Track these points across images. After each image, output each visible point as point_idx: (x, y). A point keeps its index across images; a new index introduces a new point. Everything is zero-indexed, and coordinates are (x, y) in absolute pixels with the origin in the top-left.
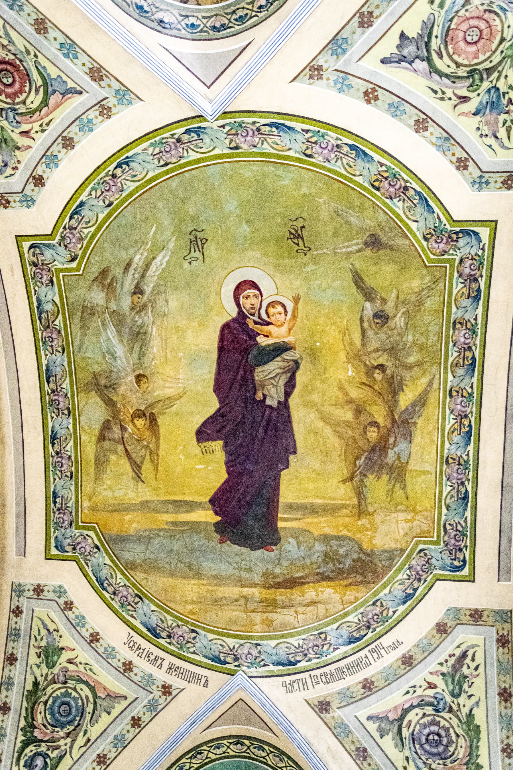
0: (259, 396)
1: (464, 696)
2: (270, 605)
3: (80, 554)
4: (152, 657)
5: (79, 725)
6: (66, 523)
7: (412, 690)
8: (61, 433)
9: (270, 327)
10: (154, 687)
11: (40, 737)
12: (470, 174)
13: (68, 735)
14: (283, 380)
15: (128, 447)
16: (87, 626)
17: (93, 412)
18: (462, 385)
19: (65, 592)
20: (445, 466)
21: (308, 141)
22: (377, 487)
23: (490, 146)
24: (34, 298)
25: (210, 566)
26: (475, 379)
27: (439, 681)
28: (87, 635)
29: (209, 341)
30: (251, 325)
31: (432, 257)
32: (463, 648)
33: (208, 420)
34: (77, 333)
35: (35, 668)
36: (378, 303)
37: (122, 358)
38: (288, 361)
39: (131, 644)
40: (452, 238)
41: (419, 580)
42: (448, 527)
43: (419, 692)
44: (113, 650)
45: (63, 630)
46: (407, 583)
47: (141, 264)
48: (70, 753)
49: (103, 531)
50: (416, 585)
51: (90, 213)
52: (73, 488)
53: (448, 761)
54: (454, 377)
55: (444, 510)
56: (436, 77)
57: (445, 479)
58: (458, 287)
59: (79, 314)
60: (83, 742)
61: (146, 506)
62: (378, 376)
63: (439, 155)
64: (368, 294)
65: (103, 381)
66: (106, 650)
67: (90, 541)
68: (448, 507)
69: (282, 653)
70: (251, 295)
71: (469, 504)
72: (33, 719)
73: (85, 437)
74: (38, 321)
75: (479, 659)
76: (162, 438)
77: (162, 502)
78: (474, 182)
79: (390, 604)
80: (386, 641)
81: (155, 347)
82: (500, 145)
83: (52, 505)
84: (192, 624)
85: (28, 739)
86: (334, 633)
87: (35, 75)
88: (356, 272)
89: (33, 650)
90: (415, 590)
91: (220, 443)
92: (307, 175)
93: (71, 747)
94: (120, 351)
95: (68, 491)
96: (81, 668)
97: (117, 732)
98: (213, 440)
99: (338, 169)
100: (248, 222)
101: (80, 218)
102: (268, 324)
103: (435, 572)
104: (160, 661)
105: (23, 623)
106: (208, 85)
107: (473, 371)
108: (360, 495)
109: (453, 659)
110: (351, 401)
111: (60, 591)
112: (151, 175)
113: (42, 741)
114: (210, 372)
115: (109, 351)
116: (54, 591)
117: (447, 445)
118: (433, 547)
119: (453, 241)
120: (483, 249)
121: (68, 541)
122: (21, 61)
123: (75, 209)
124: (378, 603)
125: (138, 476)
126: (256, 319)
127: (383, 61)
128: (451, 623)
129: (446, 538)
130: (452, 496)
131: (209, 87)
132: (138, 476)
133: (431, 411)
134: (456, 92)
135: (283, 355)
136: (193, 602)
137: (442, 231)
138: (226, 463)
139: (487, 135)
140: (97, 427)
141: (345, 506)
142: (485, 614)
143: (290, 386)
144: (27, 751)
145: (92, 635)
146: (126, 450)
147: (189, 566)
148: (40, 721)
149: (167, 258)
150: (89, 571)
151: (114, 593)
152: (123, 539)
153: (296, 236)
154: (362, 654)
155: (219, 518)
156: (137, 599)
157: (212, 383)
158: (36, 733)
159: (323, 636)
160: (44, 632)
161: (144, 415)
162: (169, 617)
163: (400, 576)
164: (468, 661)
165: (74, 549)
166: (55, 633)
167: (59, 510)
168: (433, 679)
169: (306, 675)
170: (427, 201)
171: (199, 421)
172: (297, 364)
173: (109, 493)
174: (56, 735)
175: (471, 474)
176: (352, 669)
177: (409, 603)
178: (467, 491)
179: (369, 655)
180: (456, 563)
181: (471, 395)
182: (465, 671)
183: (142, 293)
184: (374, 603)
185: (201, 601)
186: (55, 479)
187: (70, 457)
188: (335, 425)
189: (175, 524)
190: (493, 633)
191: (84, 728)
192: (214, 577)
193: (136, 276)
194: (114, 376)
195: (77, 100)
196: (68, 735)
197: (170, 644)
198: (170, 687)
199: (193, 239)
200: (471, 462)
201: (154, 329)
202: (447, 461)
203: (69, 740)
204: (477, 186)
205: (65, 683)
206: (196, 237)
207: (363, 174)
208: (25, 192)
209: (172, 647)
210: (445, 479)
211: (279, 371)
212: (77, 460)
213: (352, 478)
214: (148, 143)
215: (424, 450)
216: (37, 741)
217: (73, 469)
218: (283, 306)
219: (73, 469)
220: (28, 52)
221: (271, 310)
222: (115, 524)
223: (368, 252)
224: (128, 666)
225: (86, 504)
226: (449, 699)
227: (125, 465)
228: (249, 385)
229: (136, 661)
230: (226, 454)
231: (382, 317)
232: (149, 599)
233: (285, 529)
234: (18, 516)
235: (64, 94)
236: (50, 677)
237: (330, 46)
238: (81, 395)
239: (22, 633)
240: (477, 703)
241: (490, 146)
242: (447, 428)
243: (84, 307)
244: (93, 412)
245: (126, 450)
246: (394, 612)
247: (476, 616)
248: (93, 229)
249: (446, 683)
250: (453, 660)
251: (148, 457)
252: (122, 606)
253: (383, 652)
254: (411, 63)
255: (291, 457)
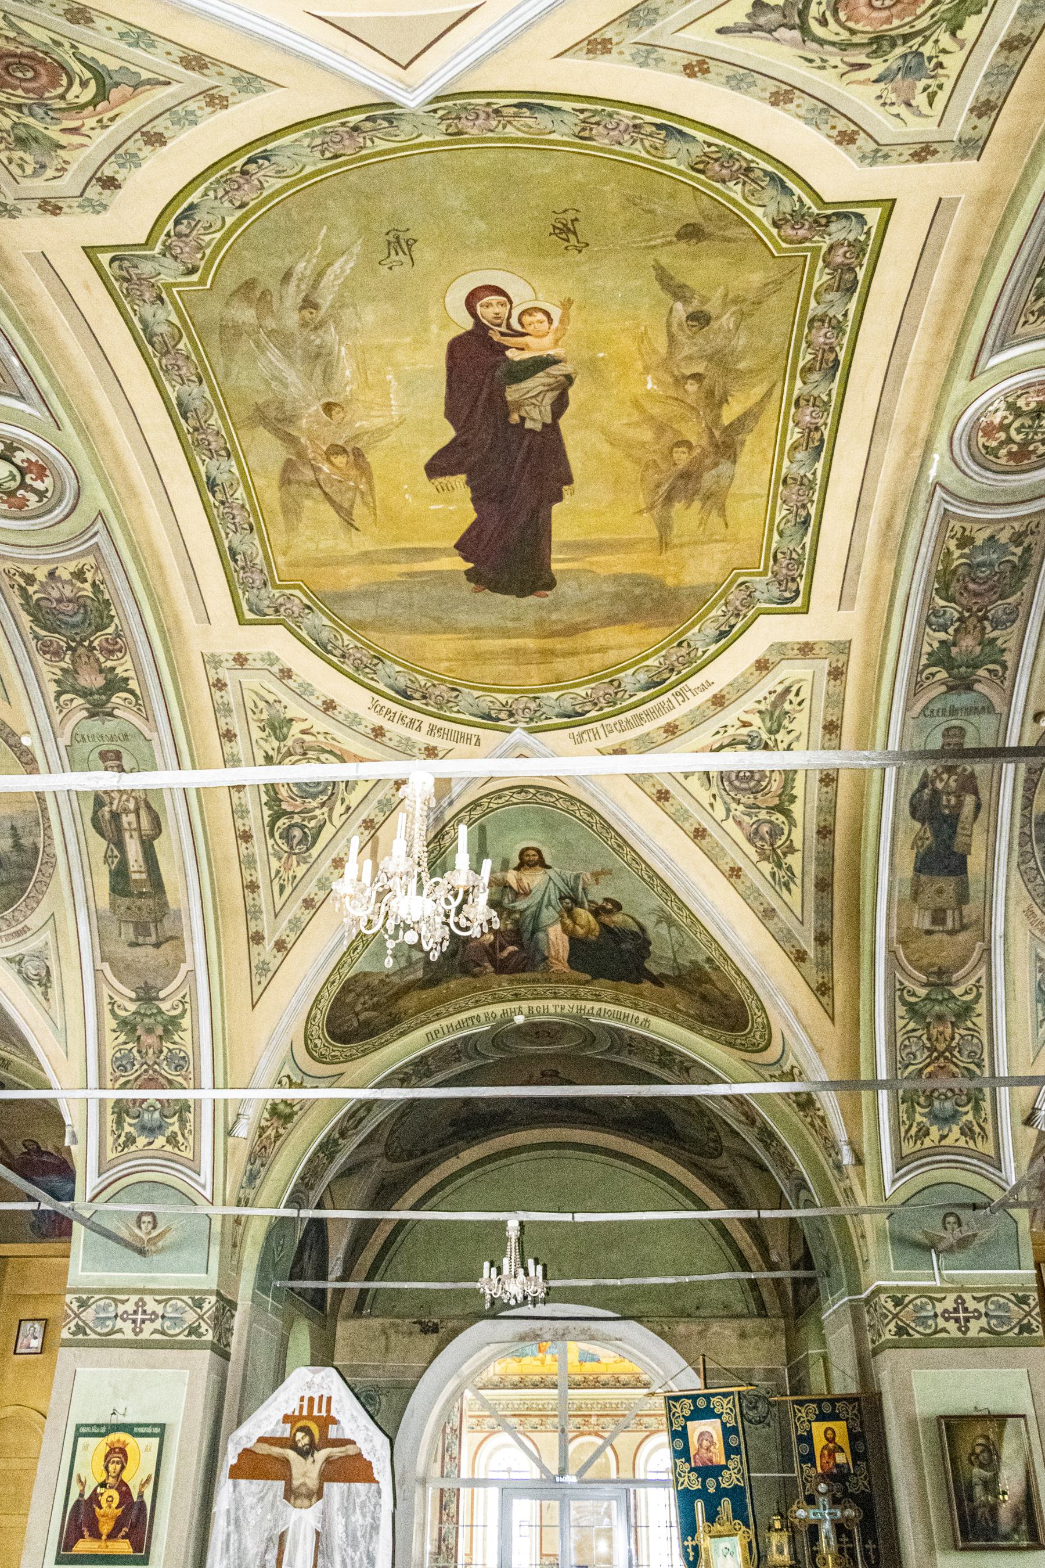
0: (515, 418)
1: (782, 731)
2: (546, 655)
3: (289, 616)
4: (407, 720)
5: (332, 794)
6: (258, 583)
7: (722, 731)
8: (222, 478)
9: (527, 339)
10: (416, 751)
11: (289, 809)
12: (859, 148)
13: (323, 804)
14: (550, 398)
15: (327, 490)
16: (316, 694)
17: (265, 452)
18: (815, 393)
19: (277, 659)
20: (781, 487)
21: (584, 122)
22: (686, 517)
23: (898, 116)
24: (136, 320)
25: (464, 618)
26: (835, 385)
27: (756, 720)
28: (319, 703)
29: (432, 364)
30: (497, 338)
31: (784, 245)
32: (787, 684)
33: (440, 451)
34: (220, 362)
35: (262, 742)
36: (696, 302)
37: (295, 383)
38: (555, 376)
39: (375, 707)
40: (821, 223)
41: (738, 615)
42: (779, 556)
43: (731, 731)
44: (356, 716)
45: (285, 700)
46: (722, 619)
47: (308, 272)
48: (331, 821)
49: (313, 588)
50: (733, 621)
51: (210, 218)
52: (257, 542)
53: (759, 795)
54: (805, 383)
55: (776, 537)
56: (814, 46)
57: (779, 501)
58: (822, 277)
59: (216, 337)
60: (343, 810)
61: (366, 557)
62: (692, 387)
63: (811, 130)
64: (679, 292)
65: (272, 413)
66: (347, 717)
67: (297, 601)
68: (781, 534)
69: (567, 704)
70: (494, 303)
71: (810, 529)
72: (276, 793)
73: (260, 482)
74: (149, 347)
75: (805, 694)
76: (375, 477)
77: (389, 551)
78: (864, 157)
79: (699, 644)
80: (693, 682)
81: (347, 370)
82: (913, 113)
83: (232, 564)
84: (452, 683)
85: (276, 812)
86: (630, 680)
87: (77, 67)
88: (662, 268)
89: (254, 726)
90: (732, 627)
91: (462, 478)
92: (583, 161)
93: (330, 817)
94: (291, 376)
95: (250, 546)
96: (321, 738)
97: (380, 796)
98: (452, 474)
99: (636, 153)
100: (482, 217)
101: (193, 223)
102: (523, 335)
103: (758, 605)
104: (417, 724)
105: (231, 696)
106: (404, 64)
107: (834, 375)
108: (664, 527)
109: (774, 696)
110: (652, 418)
111: (271, 660)
112: (308, 170)
113: (293, 812)
114: (437, 395)
115: (275, 378)
116: (263, 660)
117: (786, 462)
118: (758, 579)
119: (820, 225)
120: (868, 233)
121: (267, 602)
122: (46, 53)
123: (180, 213)
124: (685, 644)
125: (350, 523)
126: (503, 329)
127: (720, 31)
128: (772, 659)
129: (776, 568)
130: (788, 521)
131: (405, 68)
132: (350, 523)
133: (768, 421)
134: (846, 59)
135: (548, 370)
136: (449, 660)
137: (803, 216)
138: (473, 500)
139: (893, 104)
140: (276, 470)
141: (642, 541)
142: (817, 648)
143: (560, 405)
144: (279, 823)
145: (324, 703)
146: (326, 494)
147: (438, 620)
148: (285, 794)
149: (352, 265)
150: (304, 634)
151: (344, 656)
152: (343, 597)
153: (565, 230)
154: (664, 698)
155: (471, 565)
156: (376, 661)
157: (443, 408)
158: (284, 806)
159: (616, 683)
160: (262, 705)
161: (345, 451)
162: (420, 677)
163: (713, 613)
164: (791, 696)
165: (277, 611)
166: (277, 705)
167: (243, 568)
168: (746, 718)
169: (598, 724)
170: (782, 182)
171: (427, 453)
172: (569, 379)
173: (311, 545)
174: (309, 806)
175: (816, 494)
176: (650, 715)
177: (723, 641)
178: (809, 515)
179: (672, 699)
180: (787, 595)
181: (826, 404)
182: (787, 706)
183: (316, 307)
184: (680, 645)
185: (461, 657)
186: (227, 534)
187: (243, 507)
188: (627, 446)
189: (411, 575)
190: (825, 666)
191: (340, 797)
192: (471, 630)
193: (303, 287)
194: (288, 406)
195: (161, 92)
196: (323, 804)
197: (427, 704)
198: (435, 748)
199: (392, 240)
200: (818, 482)
201: (343, 349)
202: (785, 482)
203: (325, 809)
204: (868, 161)
205: (305, 754)
206: (398, 238)
207: (676, 158)
208: (86, 195)
209: (430, 708)
210: (779, 501)
211: (541, 388)
212: (255, 508)
213: (650, 508)
214: (301, 133)
215: (752, 473)
216: (285, 813)
217: (252, 520)
218: (547, 314)
219: (252, 520)
220: (59, 44)
221: (527, 319)
222: (327, 581)
223: (682, 245)
224: (378, 732)
225: (280, 560)
226: (765, 736)
227: (327, 511)
228: (500, 408)
229: (387, 725)
230: (473, 490)
231: (700, 319)
232: (390, 659)
233: (562, 571)
234: (185, 578)
235: (135, 87)
236: (284, 750)
237: (627, 16)
238: (241, 432)
239: (233, 706)
240: (798, 738)
241: (898, 116)
242: (789, 443)
243: (223, 328)
244: (265, 452)
245: (326, 494)
246: (704, 652)
247: (806, 649)
248: (218, 235)
249: (763, 720)
250: (773, 696)
251: (358, 499)
252: (357, 669)
253: (689, 694)
254: (770, 32)
255: (566, 487)
